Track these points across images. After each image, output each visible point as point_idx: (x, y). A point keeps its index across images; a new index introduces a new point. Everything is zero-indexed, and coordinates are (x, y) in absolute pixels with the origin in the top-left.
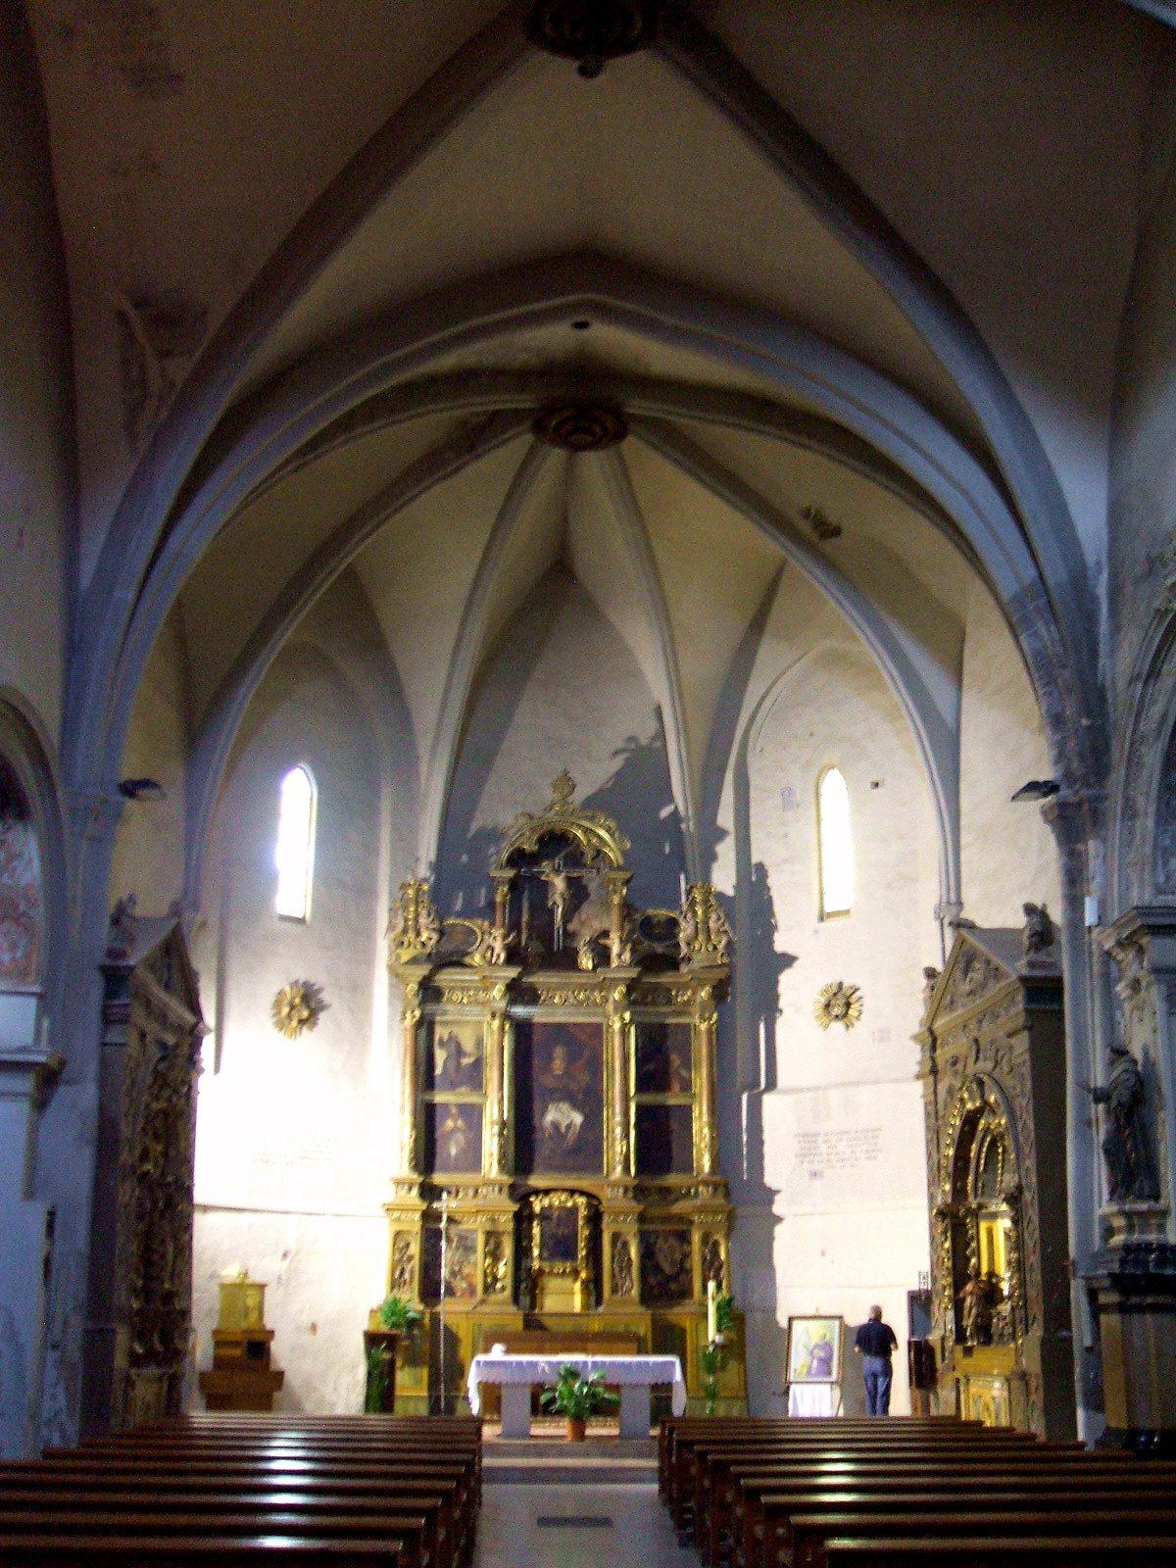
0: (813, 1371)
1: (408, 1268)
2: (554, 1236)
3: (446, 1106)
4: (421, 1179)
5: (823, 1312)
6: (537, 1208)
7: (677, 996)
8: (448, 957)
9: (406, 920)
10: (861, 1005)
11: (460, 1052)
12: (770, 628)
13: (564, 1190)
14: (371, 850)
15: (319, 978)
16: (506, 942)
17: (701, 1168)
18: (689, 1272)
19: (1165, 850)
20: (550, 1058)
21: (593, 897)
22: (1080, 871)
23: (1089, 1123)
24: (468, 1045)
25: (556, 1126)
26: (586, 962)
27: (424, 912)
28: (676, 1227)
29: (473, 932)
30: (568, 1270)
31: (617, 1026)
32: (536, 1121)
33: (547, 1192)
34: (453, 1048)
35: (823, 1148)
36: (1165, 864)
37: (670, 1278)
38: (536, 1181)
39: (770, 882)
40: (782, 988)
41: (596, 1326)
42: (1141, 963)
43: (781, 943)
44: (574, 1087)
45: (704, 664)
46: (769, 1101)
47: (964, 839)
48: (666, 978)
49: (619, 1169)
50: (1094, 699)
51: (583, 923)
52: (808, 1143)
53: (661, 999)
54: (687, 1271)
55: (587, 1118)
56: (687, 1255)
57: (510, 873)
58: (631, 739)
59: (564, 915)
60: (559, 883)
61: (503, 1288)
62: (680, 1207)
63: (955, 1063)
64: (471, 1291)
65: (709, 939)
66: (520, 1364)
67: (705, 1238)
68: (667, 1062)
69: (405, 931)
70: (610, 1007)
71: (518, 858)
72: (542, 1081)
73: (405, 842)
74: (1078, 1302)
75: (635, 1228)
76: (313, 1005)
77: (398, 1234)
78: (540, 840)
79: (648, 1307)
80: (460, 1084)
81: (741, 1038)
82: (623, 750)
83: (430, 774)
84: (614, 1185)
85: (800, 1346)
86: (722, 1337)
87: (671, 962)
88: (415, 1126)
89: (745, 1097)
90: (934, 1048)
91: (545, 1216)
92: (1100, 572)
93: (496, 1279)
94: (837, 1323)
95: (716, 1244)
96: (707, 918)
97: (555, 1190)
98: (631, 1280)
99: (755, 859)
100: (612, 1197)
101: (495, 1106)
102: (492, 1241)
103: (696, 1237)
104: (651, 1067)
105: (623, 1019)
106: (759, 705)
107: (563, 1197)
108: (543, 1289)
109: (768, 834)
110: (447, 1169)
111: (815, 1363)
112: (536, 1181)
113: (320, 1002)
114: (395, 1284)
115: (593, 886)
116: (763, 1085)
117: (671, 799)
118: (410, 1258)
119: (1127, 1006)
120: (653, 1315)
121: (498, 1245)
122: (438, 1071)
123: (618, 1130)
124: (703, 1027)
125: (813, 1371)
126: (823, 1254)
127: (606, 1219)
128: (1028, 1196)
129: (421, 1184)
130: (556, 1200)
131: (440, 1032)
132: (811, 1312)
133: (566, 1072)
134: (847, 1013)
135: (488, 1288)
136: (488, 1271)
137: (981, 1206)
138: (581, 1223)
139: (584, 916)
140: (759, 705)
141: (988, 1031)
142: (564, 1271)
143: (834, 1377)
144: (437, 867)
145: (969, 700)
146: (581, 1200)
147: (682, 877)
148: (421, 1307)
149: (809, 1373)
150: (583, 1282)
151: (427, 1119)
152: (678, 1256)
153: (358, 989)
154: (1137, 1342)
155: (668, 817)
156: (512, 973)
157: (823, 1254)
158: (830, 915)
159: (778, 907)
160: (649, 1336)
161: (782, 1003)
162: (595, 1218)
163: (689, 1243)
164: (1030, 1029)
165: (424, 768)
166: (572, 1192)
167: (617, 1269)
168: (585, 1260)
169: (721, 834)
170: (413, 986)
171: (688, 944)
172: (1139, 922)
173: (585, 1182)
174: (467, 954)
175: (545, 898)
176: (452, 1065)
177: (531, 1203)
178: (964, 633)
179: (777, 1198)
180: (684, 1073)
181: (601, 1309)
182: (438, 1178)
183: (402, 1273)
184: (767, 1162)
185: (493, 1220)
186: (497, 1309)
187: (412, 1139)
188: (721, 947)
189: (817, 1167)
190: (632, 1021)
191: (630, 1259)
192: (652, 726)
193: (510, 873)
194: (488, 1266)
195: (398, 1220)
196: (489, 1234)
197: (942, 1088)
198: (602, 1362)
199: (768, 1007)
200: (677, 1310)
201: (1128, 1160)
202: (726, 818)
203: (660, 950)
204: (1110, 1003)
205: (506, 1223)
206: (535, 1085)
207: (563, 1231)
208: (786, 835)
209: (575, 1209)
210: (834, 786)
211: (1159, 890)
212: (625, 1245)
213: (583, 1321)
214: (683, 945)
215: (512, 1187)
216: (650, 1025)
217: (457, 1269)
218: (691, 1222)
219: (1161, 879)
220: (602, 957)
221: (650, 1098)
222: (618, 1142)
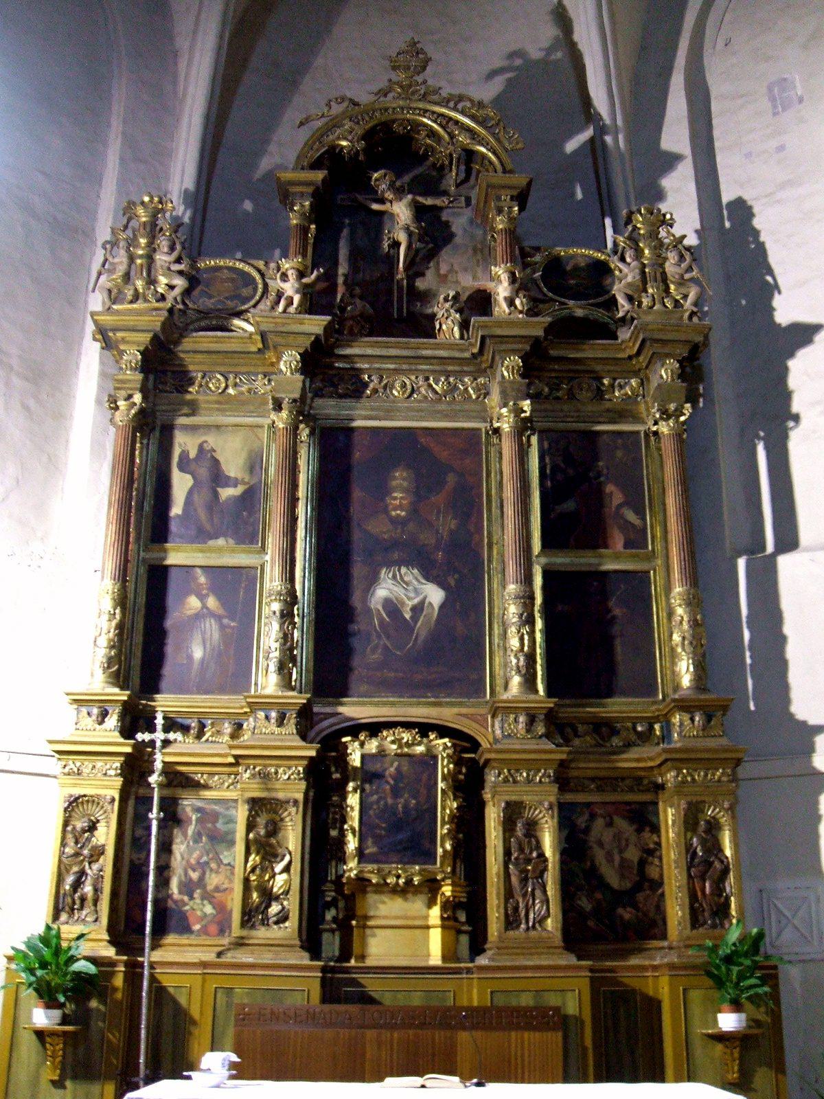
2: (388, 811)
4: (124, 696)
6: (355, 759)
7: (612, 386)
11: (218, 477)
13: (408, 726)
14: (91, 175)
16: (305, 280)
18: (657, 884)
20: (382, 491)
21: (458, 240)
24: (233, 466)
25: (392, 607)
26: (449, 326)
28: (630, 797)
30: (416, 880)
32: (356, 600)
33: (374, 729)
34: (203, 472)
37: (626, 897)
38: (353, 710)
39: (757, 223)
40: (793, 382)
41: (474, 995)
44: (427, 538)
46: (786, 564)
48: (593, 350)
49: (516, 680)
51: (443, 279)
53: (585, 395)
54: (652, 881)
56: (652, 852)
58: (513, 55)
59: (409, 265)
60: (401, 211)
61: (283, 918)
67: (691, 820)
70: (495, 398)
75: (551, 794)
77: (74, 804)
78: (368, 136)
82: (501, 71)
86: (743, 1016)
88: (122, 601)
89: (741, 563)
91: (369, 775)
93: (268, 896)
95: (713, 828)
102: (261, 821)
103: (670, 816)
105: (518, 411)
107: (406, 736)
109: (748, 155)
110: (181, 689)
112: (353, 710)
115: (459, 222)
116: (770, 547)
118: (98, 852)
121: (274, 829)
122: (176, 510)
123: (513, 610)
129: (125, 704)
130: (389, 741)
131: (184, 443)
133: (414, 511)
135: (251, 916)
136: (253, 878)
138: (441, 785)
139: (444, 269)
142: (409, 882)
146: (442, 745)
150: (444, 908)
152: (633, 854)
156: (316, 324)
159: (775, 257)
163: (655, 829)
167: (514, 880)
168: (449, 861)
169: (670, 161)
170: (132, 355)
171: (630, 299)
173: (447, 714)
177: (345, 746)
180: (631, 516)
181: (482, 961)
183: (77, 885)
184: (795, 676)
186: (267, 957)
191: (541, 855)
192: (549, 32)
194: (253, 870)
196: (256, 805)
203: (579, 313)
206: (357, 536)
208: (781, 148)
209: (430, 759)
212: (532, 828)
213: (447, 984)
214: (621, 300)
216: (566, 433)
217: (195, 876)
221: (563, 560)
222: (513, 630)
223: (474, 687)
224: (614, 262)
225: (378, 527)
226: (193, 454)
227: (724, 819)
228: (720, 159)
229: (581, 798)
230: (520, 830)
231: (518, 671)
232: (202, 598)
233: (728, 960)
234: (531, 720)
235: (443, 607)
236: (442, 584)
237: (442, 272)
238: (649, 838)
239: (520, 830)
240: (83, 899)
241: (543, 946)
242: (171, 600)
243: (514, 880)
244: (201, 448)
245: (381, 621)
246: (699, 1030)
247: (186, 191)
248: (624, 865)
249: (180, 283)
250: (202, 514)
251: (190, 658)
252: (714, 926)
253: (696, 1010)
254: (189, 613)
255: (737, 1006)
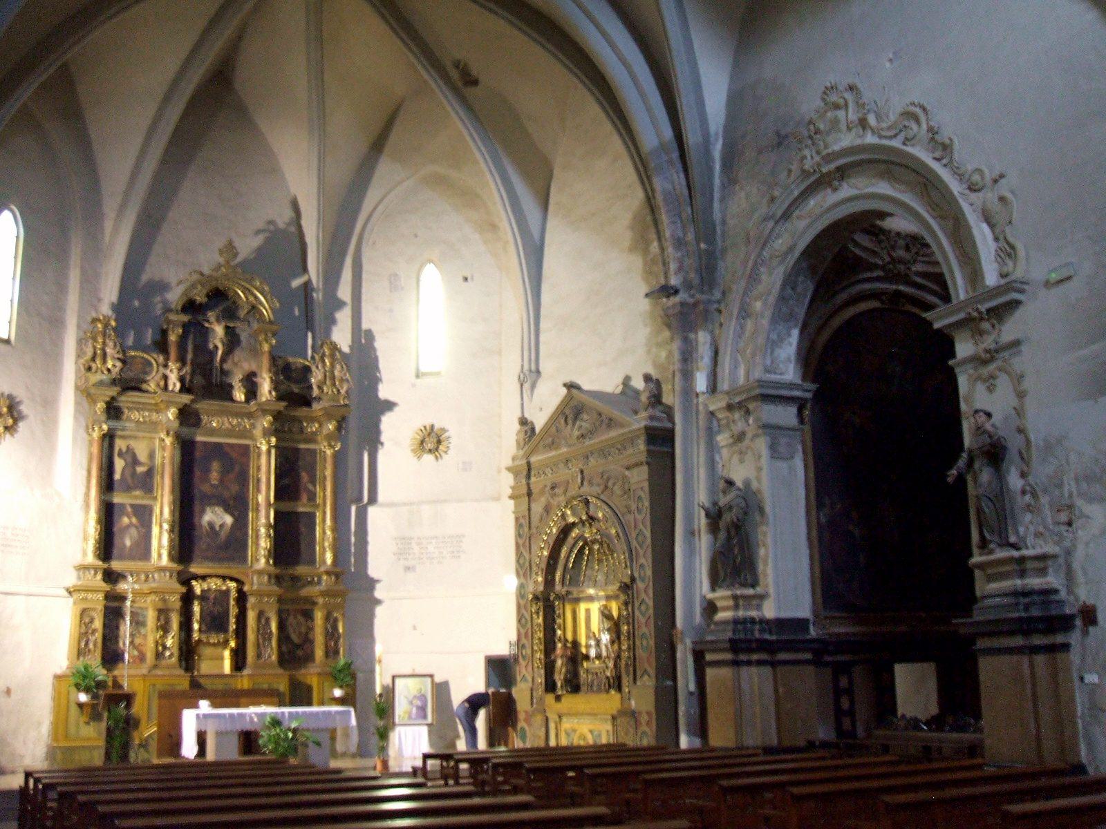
0: (413, 716)
1: (92, 638)
3: (122, 506)
5: (418, 671)
6: (198, 590)
8: (130, 383)
9: (95, 348)
10: (450, 443)
11: (135, 462)
12: (387, 149)
13: (217, 576)
14: (62, 288)
15: (20, 393)
17: (324, 562)
18: (312, 642)
19: (773, 342)
20: (207, 471)
22: (691, 353)
23: (692, 533)
24: (142, 456)
26: (239, 395)
27: (111, 344)
29: (150, 364)
31: (264, 448)
32: (196, 520)
33: (204, 578)
34: (129, 459)
35: (416, 549)
36: (772, 352)
37: (299, 646)
38: (195, 569)
39: (377, 345)
42: (747, 421)
43: (384, 392)
44: (226, 494)
45: (342, 169)
46: (372, 511)
47: (542, 325)
50: (706, 229)
51: (235, 364)
52: (404, 545)
55: (236, 520)
56: (311, 629)
57: (185, 318)
58: (271, 222)
60: (219, 330)
62: (305, 592)
63: (553, 488)
64: (142, 658)
65: (334, 384)
66: (231, 715)
68: (298, 476)
69: (93, 359)
71: (190, 306)
72: (202, 488)
73: (90, 283)
74: (685, 662)
75: (275, 607)
76: (15, 414)
77: (83, 612)
78: (208, 296)
79: (285, 669)
80: (136, 488)
81: (351, 463)
83: (116, 229)
84: (260, 573)
85: (402, 697)
87: (305, 400)
89: (353, 509)
90: (528, 476)
91: (204, 597)
92: (717, 140)
93: (165, 647)
94: (429, 680)
95: (336, 620)
96: (333, 366)
97: (210, 576)
98: (272, 649)
99: (365, 326)
100: (254, 584)
101: (163, 508)
102: (162, 618)
103: (319, 616)
104: (286, 481)
106: (375, 208)
108: (199, 657)
111: (414, 710)
112: (195, 569)
113: (20, 412)
114: (81, 653)
115: (244, 336)
117: (305, 269)
118: (94, 631)
119: (725, 452)
120: (290, 675)
121: (168, 621)
122: (117, 476)
124: (329, 452)
125: (413, 716)
126: (415, 628)
127: (252, 600)
128: (640, 585)
131: (120, 444)
132: (408, 671)
133: (221, 481)
134: (438, 447)
135: (159, 656)
137: (568, 593)
139: (236, 359)
140: (375, 208)
141: (614, 466)
142: (219, 641)
143: (429, 720)
144: (118, 308)
145: (552, 223)
146: (233, 585)
147: (310, 335)
148: (105, 672)
149: (410, 717)
151: (108, 515)
152: (303, 630)
153: (49, 404)
154: (745, 686)
155: (298, 288)
156: (186, 399)
157: (415, 628)
158: (425, 374)
159: (382, 364)
160: (287, 693)
161: (383, 438)
162: (242, 598)
164: (648, 463)
165: (108, 225)
166: (224, 578)
167: (261, 641)
169: (340, 304)
170: (101, 406)
171: (319, 387)
172: (757, 391)
174: (145, 382)
175: (206, 341)
176: (128, 473)
178: (551, 171)
179: (378, 586)
180: (310, 487)
182: (116, 565)
183: (87, 644)
185: (164, 600)
186: (167, 672)
187: (97, 533)
188: (343, 391)
189: (410, 563)
190: (276, 447)
191: (271, 631)
192: (288, 214)
193: (185, 318)
195: (85, 599)
197: (538, 508)
198: (229, 714)
199: (373, 440)
200: (303, 671)
201: (735, 562)
202: (344, 292)
204: (712, 448)
205: (175, 601)
206: (196, 491)
207: (217, 609)
209: (228, 591)
210: (431, 275)
211: (767, 371)
212: (268, 621)
213: (232, 681)
214: (315, 387)
215: (179, 573)
216: (286, 448)
218: (314, 604)
219: (768, 362)
220: (252, 392)
223: (243, 559)
224: (314, 368)
225: (205, 488)
226: (124, 450)
227: (340, 617)
228: (363, 304)
229: (286, 607)
230: (263, 621)
231: (265, 557)
232: (129, 517)
233: (340, 671)
234: (270, 577)
235: (233, 525)
236: (232, 515)
237: (235, 361)
238: (309, 623)
239: (263, 621)
240: (89, 651)
241: (271, 666)
242: (116, 518)
243: (261, 641)
244: (128, 447)
245: (207, 530)
246: (327, 696)
247: (113, 303)
248: (300, 633)
249: (119, 364)
250: (130, 481)
251: (124, 545)
252: (334, 659)
253: (326, 689)
254: (124, 525)
255: (341, 687)
